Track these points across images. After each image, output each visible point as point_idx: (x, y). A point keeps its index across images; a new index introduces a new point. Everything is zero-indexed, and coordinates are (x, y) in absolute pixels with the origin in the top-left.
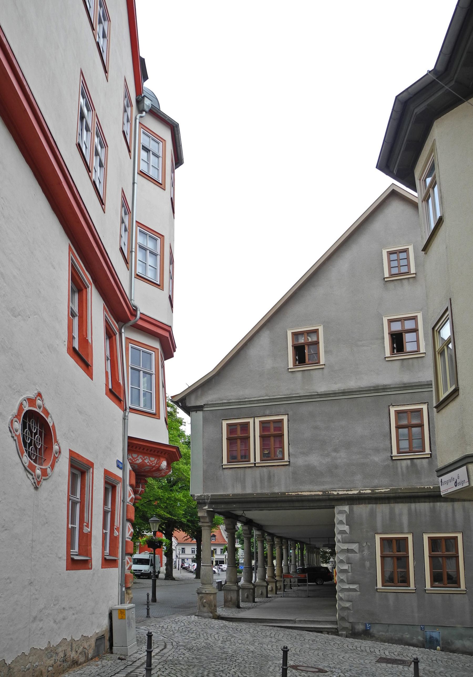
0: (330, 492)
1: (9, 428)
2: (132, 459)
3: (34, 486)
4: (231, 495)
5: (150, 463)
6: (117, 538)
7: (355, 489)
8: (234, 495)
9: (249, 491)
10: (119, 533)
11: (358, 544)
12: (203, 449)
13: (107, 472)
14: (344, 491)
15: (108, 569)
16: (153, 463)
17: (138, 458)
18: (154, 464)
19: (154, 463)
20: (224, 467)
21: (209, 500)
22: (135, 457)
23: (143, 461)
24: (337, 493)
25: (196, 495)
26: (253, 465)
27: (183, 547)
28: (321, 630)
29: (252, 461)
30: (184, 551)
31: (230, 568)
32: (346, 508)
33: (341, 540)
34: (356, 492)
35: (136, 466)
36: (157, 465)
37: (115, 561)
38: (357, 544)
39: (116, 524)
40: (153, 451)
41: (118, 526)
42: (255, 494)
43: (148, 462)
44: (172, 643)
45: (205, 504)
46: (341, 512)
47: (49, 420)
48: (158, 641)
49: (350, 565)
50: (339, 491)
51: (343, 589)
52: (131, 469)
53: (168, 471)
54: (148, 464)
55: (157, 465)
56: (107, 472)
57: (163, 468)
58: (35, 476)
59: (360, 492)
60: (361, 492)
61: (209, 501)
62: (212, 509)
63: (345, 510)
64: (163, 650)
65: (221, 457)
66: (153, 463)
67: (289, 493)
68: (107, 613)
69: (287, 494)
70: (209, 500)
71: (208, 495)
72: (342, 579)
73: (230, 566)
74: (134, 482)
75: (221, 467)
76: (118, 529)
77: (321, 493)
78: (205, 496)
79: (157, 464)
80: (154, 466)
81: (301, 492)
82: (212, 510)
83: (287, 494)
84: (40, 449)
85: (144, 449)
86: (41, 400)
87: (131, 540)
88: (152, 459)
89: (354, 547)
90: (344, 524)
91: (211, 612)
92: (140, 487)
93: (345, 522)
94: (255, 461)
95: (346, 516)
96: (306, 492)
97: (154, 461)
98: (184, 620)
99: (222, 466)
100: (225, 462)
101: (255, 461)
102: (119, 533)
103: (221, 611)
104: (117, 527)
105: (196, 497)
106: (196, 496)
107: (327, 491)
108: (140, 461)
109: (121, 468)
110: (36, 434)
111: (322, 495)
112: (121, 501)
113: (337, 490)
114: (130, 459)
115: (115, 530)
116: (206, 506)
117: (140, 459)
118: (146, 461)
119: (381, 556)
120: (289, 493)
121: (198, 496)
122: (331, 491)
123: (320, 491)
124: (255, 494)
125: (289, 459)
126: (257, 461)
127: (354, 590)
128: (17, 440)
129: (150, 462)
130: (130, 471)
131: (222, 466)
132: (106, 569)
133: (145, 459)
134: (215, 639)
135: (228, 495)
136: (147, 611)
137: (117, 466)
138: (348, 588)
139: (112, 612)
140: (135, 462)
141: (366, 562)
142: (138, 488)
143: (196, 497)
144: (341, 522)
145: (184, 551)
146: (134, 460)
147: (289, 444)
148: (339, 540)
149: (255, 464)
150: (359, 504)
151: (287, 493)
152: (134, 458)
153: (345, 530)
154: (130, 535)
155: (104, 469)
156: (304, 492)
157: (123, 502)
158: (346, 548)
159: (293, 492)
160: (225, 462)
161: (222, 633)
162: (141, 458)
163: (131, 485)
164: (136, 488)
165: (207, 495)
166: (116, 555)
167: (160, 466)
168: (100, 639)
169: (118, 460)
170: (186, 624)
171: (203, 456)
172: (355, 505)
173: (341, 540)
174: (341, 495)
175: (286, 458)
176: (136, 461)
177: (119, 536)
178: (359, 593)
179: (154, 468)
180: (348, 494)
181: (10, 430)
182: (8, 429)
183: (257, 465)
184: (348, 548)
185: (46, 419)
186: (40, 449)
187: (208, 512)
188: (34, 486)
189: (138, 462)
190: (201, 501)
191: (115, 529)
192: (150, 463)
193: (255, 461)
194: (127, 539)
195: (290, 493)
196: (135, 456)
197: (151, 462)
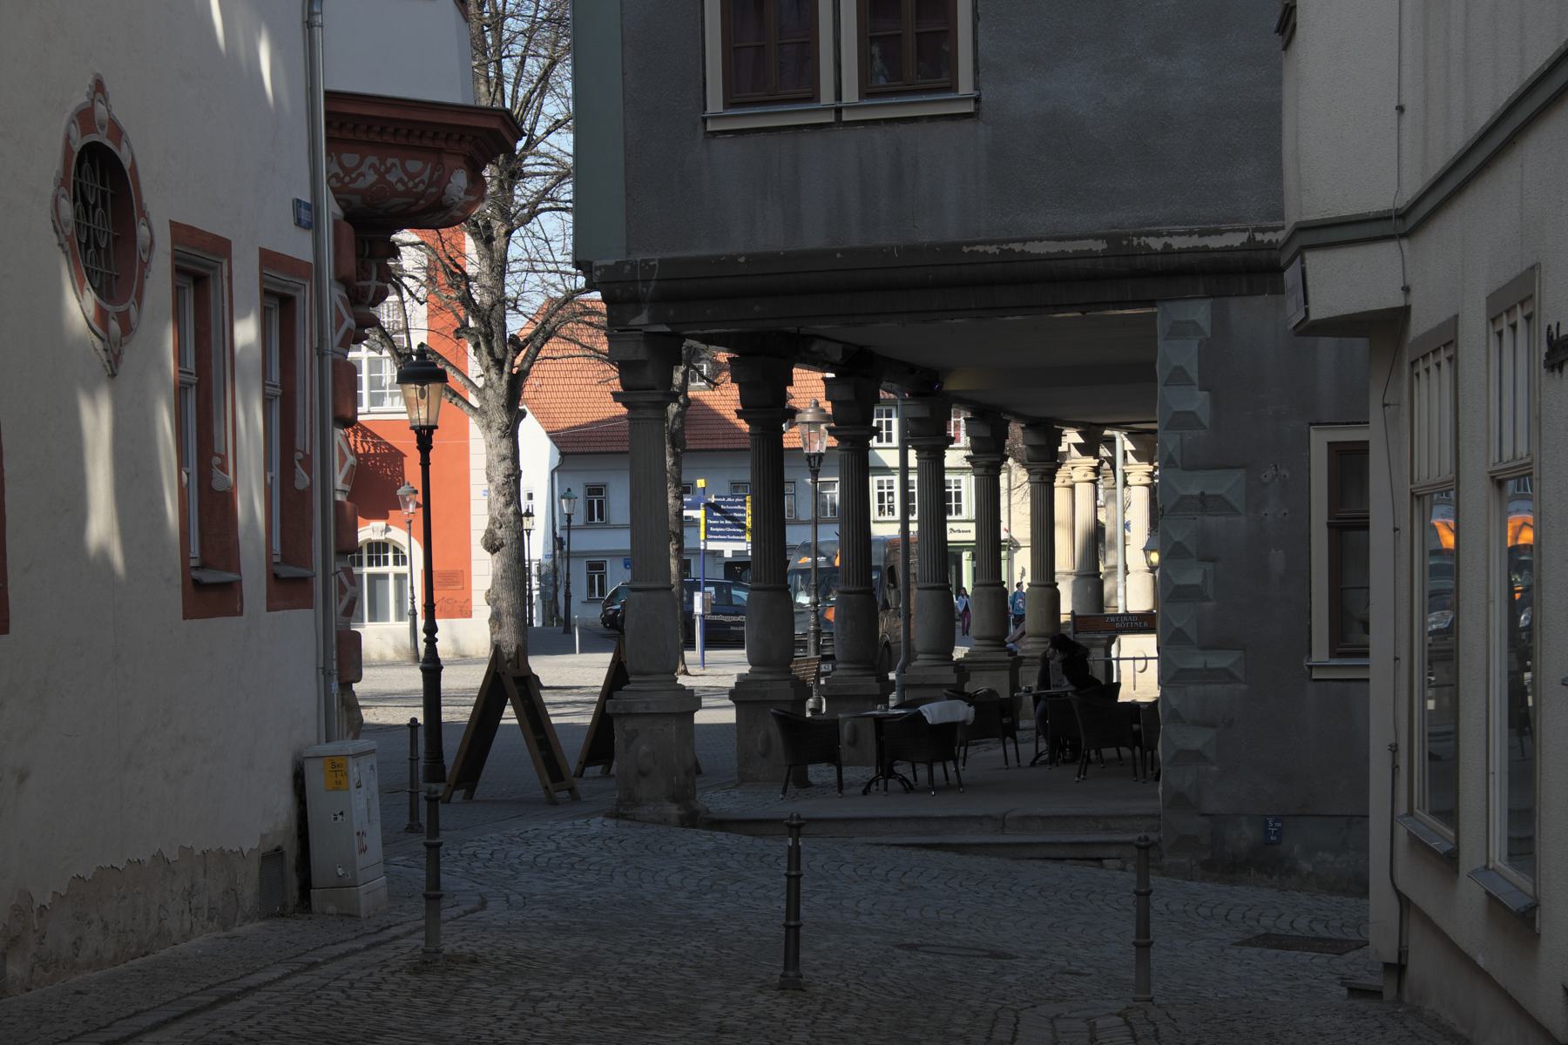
0: (1135, 242)
1: (53, 221)
2: (342, 175)
3: (107, 370)
4: (742, 260)
5: (405, 184)
6: (306, 495)
7: (1236, 226)
8: (752, 259)
9: (814, 238)
10: (311, 478)
11: (1243, 471)
12: (623, 44)
13: (269, 259)
14: (1190, 233)
15: (286, 611)
16: (417, 180)
17: (363, 169)
18: (421, 187)
19: (422, 181)
20: (711, 127)
21: (653, 284)
22: (353, 165)
23: (382, 176)
24: (1166, 245)
25: (598, 263)
26: (829, 118)
27: (595, 479)
28: (1098, 853)
29: (827, 96)
30: (600, 504)
31: (1036, 589)
32: (1199, 312)
33: (1177, 458)
34: (1236, 240)
35: (356, 199)
36: (433, 190)
37: (305, 581)
38: (1239, 474)
39: (299, 444)
40: (418, 133)
41: (308, 452)
42: (839, 255)
43: (400, 180)
44: (507, 896)
45: (636, 301)
46: (1179, 331)
47: (124, 155)
48: (456, 893)
49: (1209, 566)
50: (1170, 234)
51: (1183, 670)
52: (339, 212)
53: (472, 198)
54: (400, 187)
55: (433, 190)
56: (269, 259)
57: (457, 199)
58: (109, 342)
59: (1251, 239)
60: (1259, 237)
61: (651, 289)
62: (668, 324)
63: (1194, 322)
64: (473, 911)
65: (701, 78)
66: (417, 180)
67: (975, 248)
68: (288, 773)
69: (966, 249)
70: (653, 284)
71: (646, 262)
72: (1179, 629)
73: (761, 585)
74: (350, 266)
75: (700, 127)
76: (307, 463)
77: (1099, 246)
78: (634, 266)
79: (430, 185)
80: (422, 195)
81: (1024, 241)
82: (666, 329)
83: (966, 249)
84: (107, 249)
85: (383, 130)
86: (104, 102)
87: (349, 499)
88: (414, 166)
89: (1226, 484)
90: (1190, 382)
91: (674, 799)
92: (370, 274)
93: (1194, 374)
94: (841, 99)
95: (1199, 345)
96: (1041, 240)
97: (423, 171)
98: (561, 832)
99: (706, 123)
100: (715, 103)
101: (839, 96)
102: (310, 474)
103: (717, 801)
104: (304, 453)
105: (598, 273)
106: (597, 268)
107: (1126, 236)
108: (372, 178)
109: (308, 226)
110: (95, 207)
111: (1104, 255)
112: (315, 352)
113: (1164, 228)
114: (336, 176)
115: (297, 463)
116: (638, 313)
117: (372, 172)
118: (392, 178)
119: (1328, 523)
120: (975, 248)
121: (606, 267)
122: (1139, 236)
123: (1096, 237)
124: (842, 251)
125: (976, 87)
126: (845, 99)
127: (1225, 675)
128: (69, 253)
129: (406, 179)
130: (336, 223)
131: (705, 120)
132: (281, 612)
133: (388, 171)
134: (667, 886)
135: (732, 260)
136: (408, 798)
137: (295, 224)
138: (1202, 666)
139: (302, 769)
140: (351, 186)
141: (1273, 551)
142: (364, 279)
143: (598, 273)
144: (1179, 377)
145: (600, 504)
146: (347, 179)
147: (976, 17)
148: (1170, 456)
149: (838, 111)
150: (1251, 293)
151: (968, 244)
152: (347, 171)
153: (1193, 413)
154: (344, 481)
155: (260, 248)
156: (1033, 240)
157: (321, 354)
158: (1196, 492)
159: (991, 243)
160: (715, 103)
161: (700, 870)
162: (372, 166)
163: (342, 280)
164: (358, 280)
165: (642, 261)
166: (306, 562)
167: (443, 193)
168: (272, 857)
169: (298, 201)
170: (563, 844)
171: (624, 74)
172: (1236, 295)
173: (1177, 458)
174: (1180, 252)
175: (965, 86)
176: (354, 181)
177: (311, 485)
178: (1243, 687)
179: (422, 202)
180: (1206, 249)
181: (55, 227)
182: (51, 227)
183: (846, 117)
184: (1202, 494)
185: (117, 152)
186: (107, 249)
187: (651, 337)
188: (107, 370)
189: (361, 184)
190: (618, 291)
191: (299, 461)
192: (405, 184)
193: (839, 96)
194: (339, 497)
195: (981, 248)
196: (350, 159)
197: (412, 177)
